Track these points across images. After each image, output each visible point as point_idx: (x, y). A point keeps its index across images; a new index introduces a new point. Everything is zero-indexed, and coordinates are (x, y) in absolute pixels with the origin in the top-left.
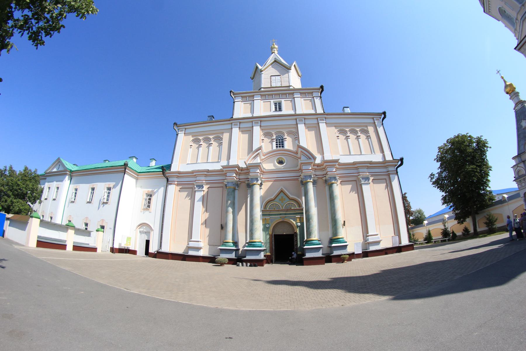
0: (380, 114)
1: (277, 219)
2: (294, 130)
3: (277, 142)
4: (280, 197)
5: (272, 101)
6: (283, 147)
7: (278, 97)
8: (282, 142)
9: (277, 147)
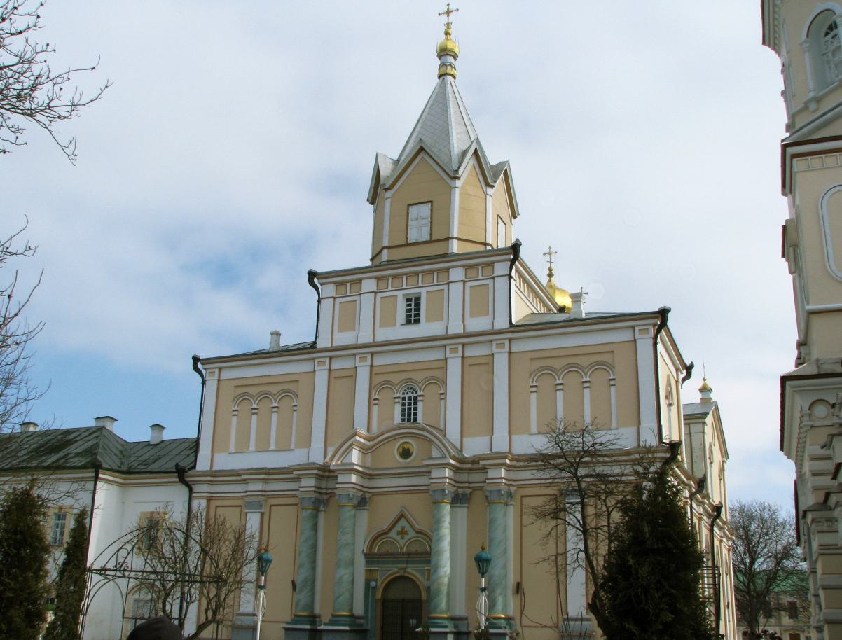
1: (393, 570)
2: (437, 373)
3: (404, 404)
4: (398, 528)
5: (400, 294)
6: (415, 420)
7: (412, 280)
8: (415, 404)
9: (403, 420)
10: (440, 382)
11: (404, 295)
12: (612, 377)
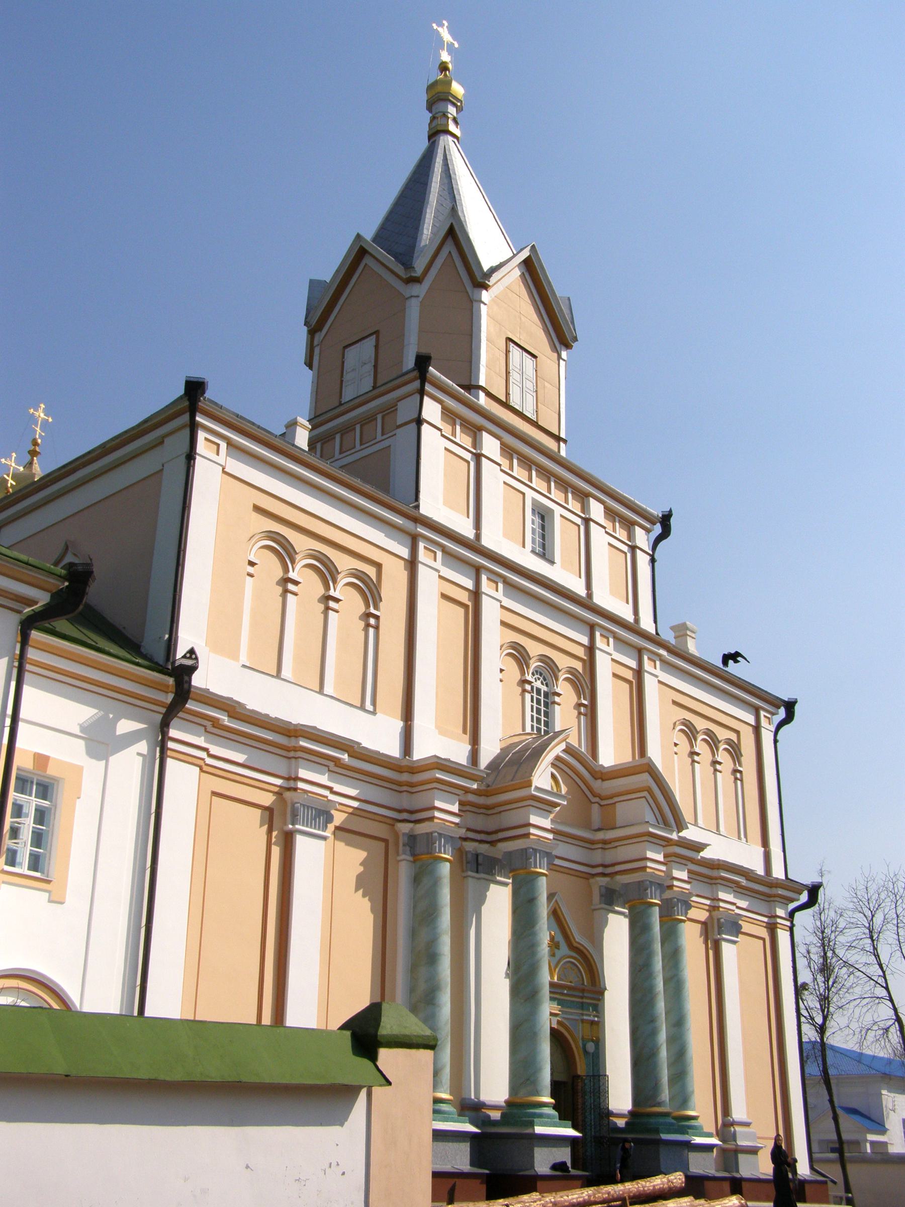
0: (774, 702)
10: (585, 683)
11: (534, 501)
12: (372, 610)
